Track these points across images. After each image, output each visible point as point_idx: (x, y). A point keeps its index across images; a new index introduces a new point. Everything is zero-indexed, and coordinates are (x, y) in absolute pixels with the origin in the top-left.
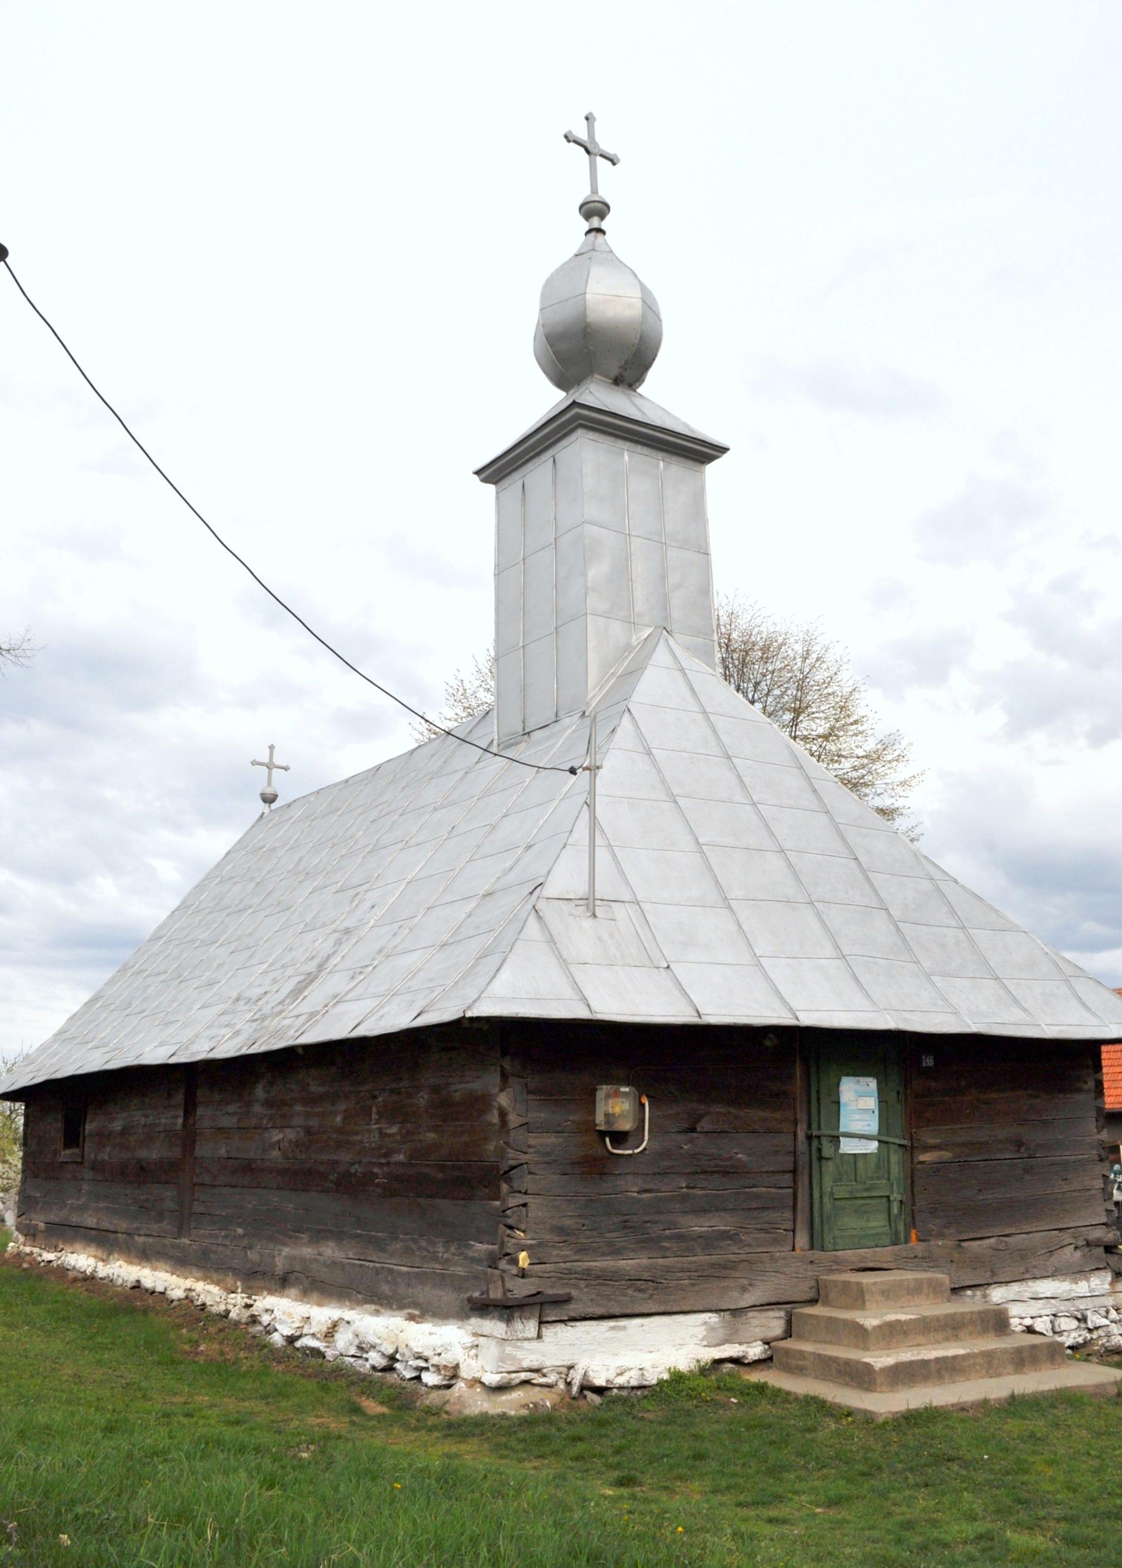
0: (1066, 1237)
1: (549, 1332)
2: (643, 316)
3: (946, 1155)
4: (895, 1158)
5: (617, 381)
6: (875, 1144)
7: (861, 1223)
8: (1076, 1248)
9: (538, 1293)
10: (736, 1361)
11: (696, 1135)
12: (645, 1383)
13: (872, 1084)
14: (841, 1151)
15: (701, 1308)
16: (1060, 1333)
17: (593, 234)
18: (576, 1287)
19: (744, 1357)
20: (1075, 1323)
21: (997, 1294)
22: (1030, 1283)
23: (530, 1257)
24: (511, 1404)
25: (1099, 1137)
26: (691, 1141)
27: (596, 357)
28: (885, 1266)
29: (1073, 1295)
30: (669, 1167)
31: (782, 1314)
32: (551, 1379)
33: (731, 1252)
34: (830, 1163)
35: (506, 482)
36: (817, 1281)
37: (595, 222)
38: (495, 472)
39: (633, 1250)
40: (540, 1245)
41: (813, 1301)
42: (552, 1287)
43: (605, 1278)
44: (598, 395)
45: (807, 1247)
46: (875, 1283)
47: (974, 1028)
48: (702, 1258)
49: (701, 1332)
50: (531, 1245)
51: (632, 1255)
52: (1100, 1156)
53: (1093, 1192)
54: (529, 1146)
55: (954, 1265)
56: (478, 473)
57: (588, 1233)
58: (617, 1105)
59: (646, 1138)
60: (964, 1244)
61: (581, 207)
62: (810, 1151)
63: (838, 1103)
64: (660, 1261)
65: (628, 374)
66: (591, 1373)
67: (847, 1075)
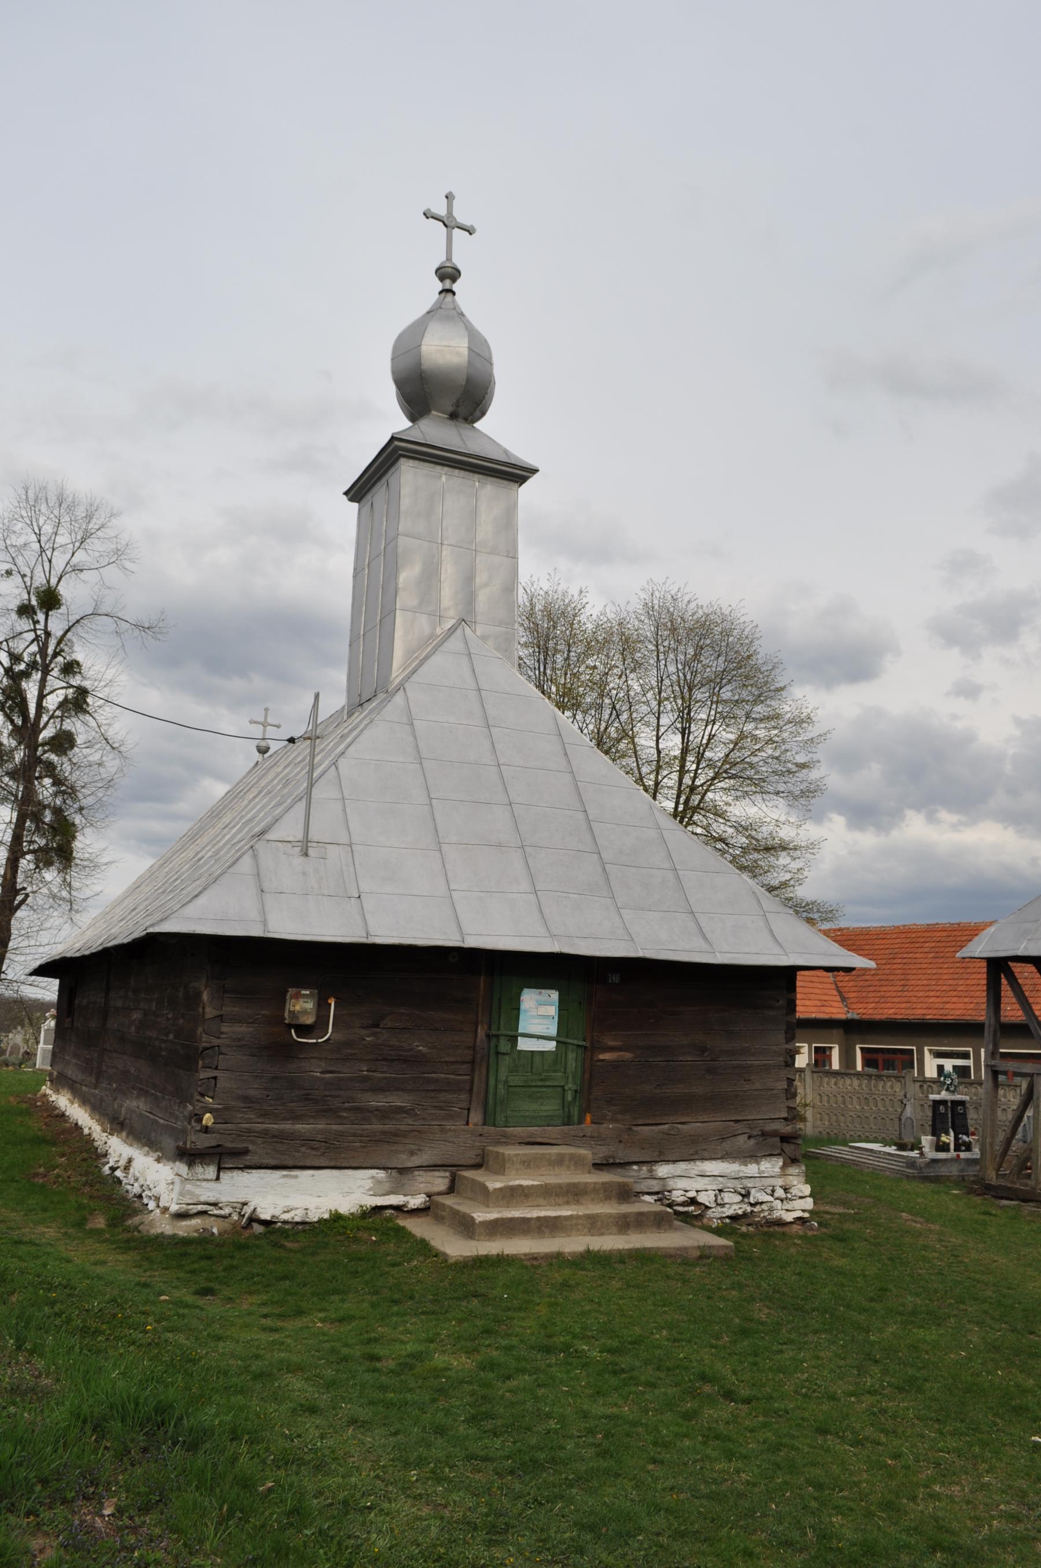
0: (740, 1127)
1: (225, 1176)
2: (469, 362)
3: (628, 1055)
4: (571, 1056)
5: (453, 416)
6: (554, 1043)
7: (535, 1106)
8: (750, 1137)
9: (219, 1146)
10: (398, 1208)
11: (378, 1030)
12: (307, 1220)
13: (555, 995)
14: (518, 1048)
15: (368, 1165)
16: (723, 1205)
17: (443, 294)
18: (253, 1143)
19: (404, 1206)
20: (739, 1198)
21: (663, 1170)
22: (698, 1163)
23: (214, 1118)
24: (185, 1228)
25: (787, 1046)
26: (374, 1034)
27: (443, 395)
28: (552, 1141)
29: (741, 1174)
30: (351, 1055)
31: (447, 1174)
32: (227, 1211)
33: (406, 1124)
34: (507, 1057)
35: (364, 501)
36: (483, 1150)
37: (447, 283)
38: (357, 492)
39: (312, 1117)
40: (226, 1109)
41: (478, 1166)
42: (232, 1142)
43: (281, 1137)
44: (436, 431)
45: (480, 1123)
46: (517, 1155)
47: (640, 954)
48: (377, 1127)
49: (369, 1184)
50: (217, 1110)
51: (311, 1121)
52: (786, 1062)
53: (775, 1092)
54: (222, 1033)
55: (622, 1145)
56: (346, 493)
57: (272, 1102)
58: (302, 1005)
59: (330, 1030)
60: (635, 1128)
61: (437, 271)
62: (489, 1047)
63: (519, 1009)
64: (334, 1127)
65: (462, 411)
66: (259, 1210)
67: (530, 986)
